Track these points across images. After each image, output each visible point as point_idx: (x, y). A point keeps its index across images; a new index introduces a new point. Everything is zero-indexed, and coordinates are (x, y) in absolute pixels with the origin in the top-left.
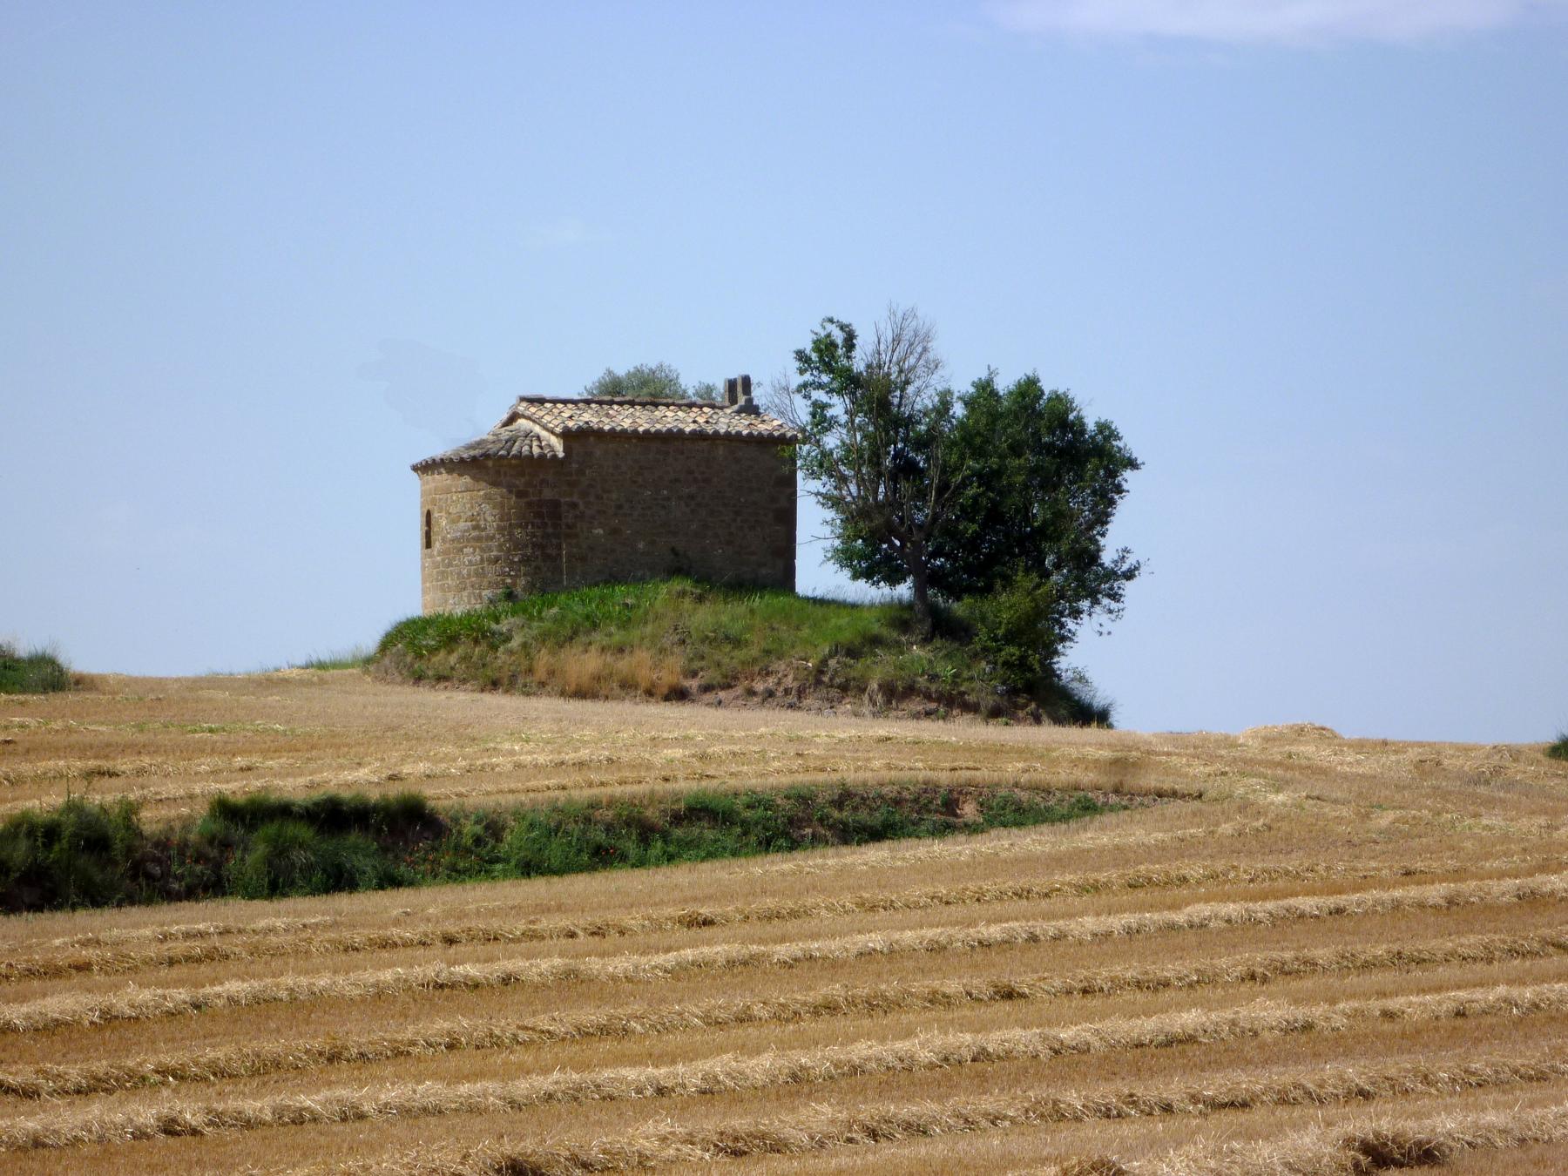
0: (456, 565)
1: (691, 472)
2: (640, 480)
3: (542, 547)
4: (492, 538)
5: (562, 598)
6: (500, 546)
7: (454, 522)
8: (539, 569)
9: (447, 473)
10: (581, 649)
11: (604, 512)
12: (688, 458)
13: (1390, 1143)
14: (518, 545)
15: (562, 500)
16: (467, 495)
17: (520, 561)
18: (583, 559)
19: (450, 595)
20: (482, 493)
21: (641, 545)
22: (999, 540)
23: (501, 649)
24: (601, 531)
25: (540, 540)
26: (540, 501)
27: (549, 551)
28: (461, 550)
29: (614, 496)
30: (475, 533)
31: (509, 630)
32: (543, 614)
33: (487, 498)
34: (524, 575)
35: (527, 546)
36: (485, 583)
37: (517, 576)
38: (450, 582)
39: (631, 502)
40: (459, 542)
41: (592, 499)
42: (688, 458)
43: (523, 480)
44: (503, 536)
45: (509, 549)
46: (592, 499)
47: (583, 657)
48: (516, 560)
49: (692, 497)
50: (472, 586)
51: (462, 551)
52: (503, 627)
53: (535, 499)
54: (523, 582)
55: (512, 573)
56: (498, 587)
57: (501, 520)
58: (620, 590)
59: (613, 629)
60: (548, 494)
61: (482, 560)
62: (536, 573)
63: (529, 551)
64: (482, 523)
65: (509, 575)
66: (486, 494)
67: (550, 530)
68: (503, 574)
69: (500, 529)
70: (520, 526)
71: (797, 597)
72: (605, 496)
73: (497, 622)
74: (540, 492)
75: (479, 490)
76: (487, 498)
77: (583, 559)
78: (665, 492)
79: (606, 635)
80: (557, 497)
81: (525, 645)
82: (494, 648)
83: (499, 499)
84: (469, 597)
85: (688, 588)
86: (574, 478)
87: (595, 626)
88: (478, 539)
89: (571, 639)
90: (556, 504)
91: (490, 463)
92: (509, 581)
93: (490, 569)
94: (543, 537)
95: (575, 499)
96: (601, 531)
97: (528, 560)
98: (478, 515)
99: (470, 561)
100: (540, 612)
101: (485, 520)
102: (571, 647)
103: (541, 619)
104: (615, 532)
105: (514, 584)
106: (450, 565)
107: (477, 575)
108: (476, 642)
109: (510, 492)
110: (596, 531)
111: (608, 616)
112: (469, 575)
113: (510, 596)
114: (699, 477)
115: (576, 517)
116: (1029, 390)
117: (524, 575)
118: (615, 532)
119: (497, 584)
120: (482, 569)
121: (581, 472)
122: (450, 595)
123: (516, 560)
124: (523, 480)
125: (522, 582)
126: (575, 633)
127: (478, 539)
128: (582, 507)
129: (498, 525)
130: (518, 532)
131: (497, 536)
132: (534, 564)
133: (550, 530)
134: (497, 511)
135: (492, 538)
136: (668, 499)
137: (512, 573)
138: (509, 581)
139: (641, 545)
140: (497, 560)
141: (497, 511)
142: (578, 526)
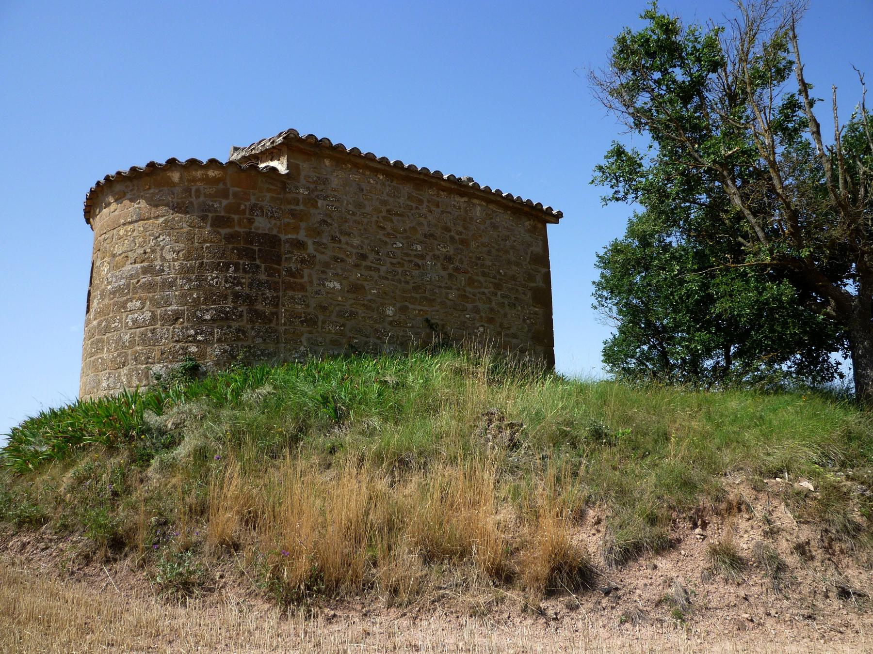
0: (116, 329)
1: (447, 229)
2: (388, 226)
3: (250, 300)
4: (172, 284)
5: (279, 373)
6: (183, 296)
7: (117, 267)
8: (244, 333)
9: (116, 201)
10: (315, 459)
11: (342, 260)
12: (443, 212)
13: (346, 490)
14: (212, 296)
15: (283, 237)
16: (139, 226)
17: (213, 320)
18: (311, 322)
19: (103, 375)
20: (161, 220)
21: (390, 311)
22: (698, 350)
23: (155, 463)
24: (338, 286)
25: (247, 290)
26: (248, 234)
27: (259, 307)
28: (124, 305)
29: (356, 242)
30: (145, 279)
31: (177, 426)
32: (245, 397)
33: (168, 227)
34: (219, 340)
35: (226, 298)
36: (156, 353)
37: (206, 342)
38: (105, 356)
39: (377, 253)
40: (123, 295)
41: (325, 240)
42: (443, 212)
43: (225, 202)
44: (189, 281)
45: (197, 302)
46: (325, 240)
47: (321, 478)
48: (207, 317)
49: (449, 259)
50: (136, 359)
51: (125, 307)
52: (168, 421)
53: (241, 230)
54: (217, 352)
55: (199, 338)
56: (175, 360)
57: (187, 258)
58: (369, 366)
59: (375, 422)
60: (261, 224)
61: (153, 318)
62: (238, 339)
63: (229, 306)
64: (158, 263)
65: (195, 341)
66: (166, 222)
67: (263, 277)
68: (187, 339)
69: (185, 271)
70: (216, 267)
71: (559, 380)
72: (343, 239)
73: (159, 411)
74: (251, 221)
75: (157, 217)
76: (168, 227)
77: (311, 322)
78: (419, 248)
79: (363, 433)
80: (275, 232)
81: (202, 455)
82: (145, 460)
83: (186, 229)
84: (129, 376)
85: (26, 540)
86: (301, 207)
87: (339, 418)
88: (150, 287)
89: (295, 439)
90: (273, 241)
91: (176, 176)
92: (193, 349)
93: (164, 331)
94: (251, 286)
95: (302, 236)
96: (338, 286)
97: (227, 319)
98: (153, 251)
99: (135, 321)
100: (237, 393)
101: (163, 259)
102: (294, 458)
103: (239, 405)
104: (356, 289)
105: (202, 355)
106: (107, 330)
107: (144, 341)
108: (112, 448)
109: (203, 218)
110: (331, 285)
111: (359, 401)
112: (132, 342)
113: (193, 372)
114: (457, 237)
115: (303, 261)
116: (604, 262)
117: (219, 340)
118: (356, 289)
119: (174, 355)
120: (153, 331)
121: (311, 202)
122: (103, 375)
123: (207, 317)
124: (225, 202)
125: (215, 351)
126: (303, 429)
127: (150, 287)
128: (311, 249)
129: (182, 267)
130: (211, 276)
131: (179, 282)
132: (235, 325)
133: (263, 277)
134: (181, 245)
135: (172, 284)
136: (422, 257)
137: (199, 338)
138: (193, 349)
139: (390, 311)
140: (176, 317)
141: (181, 245)
142: (306, 272)
